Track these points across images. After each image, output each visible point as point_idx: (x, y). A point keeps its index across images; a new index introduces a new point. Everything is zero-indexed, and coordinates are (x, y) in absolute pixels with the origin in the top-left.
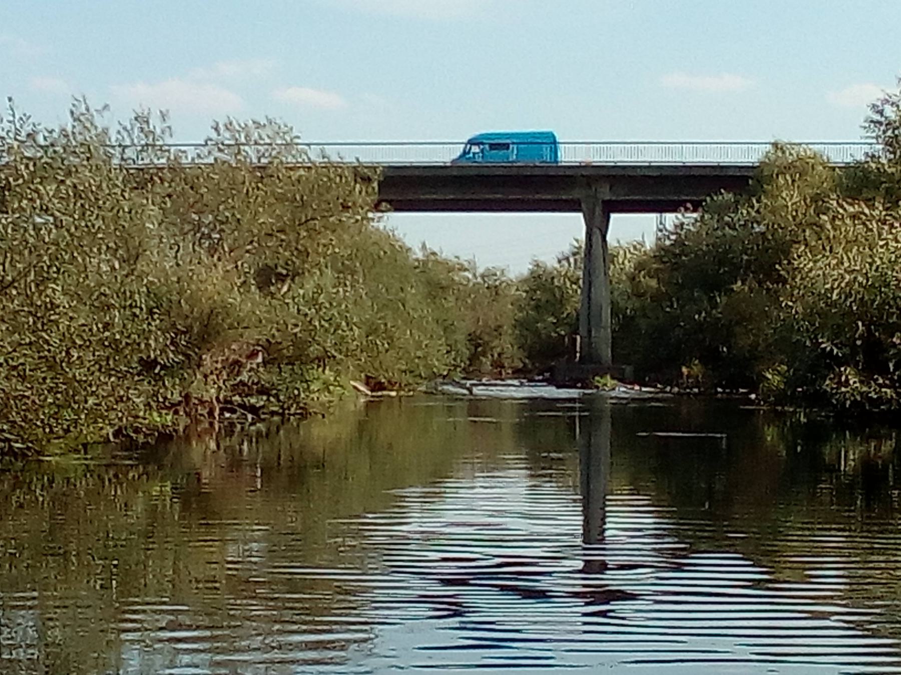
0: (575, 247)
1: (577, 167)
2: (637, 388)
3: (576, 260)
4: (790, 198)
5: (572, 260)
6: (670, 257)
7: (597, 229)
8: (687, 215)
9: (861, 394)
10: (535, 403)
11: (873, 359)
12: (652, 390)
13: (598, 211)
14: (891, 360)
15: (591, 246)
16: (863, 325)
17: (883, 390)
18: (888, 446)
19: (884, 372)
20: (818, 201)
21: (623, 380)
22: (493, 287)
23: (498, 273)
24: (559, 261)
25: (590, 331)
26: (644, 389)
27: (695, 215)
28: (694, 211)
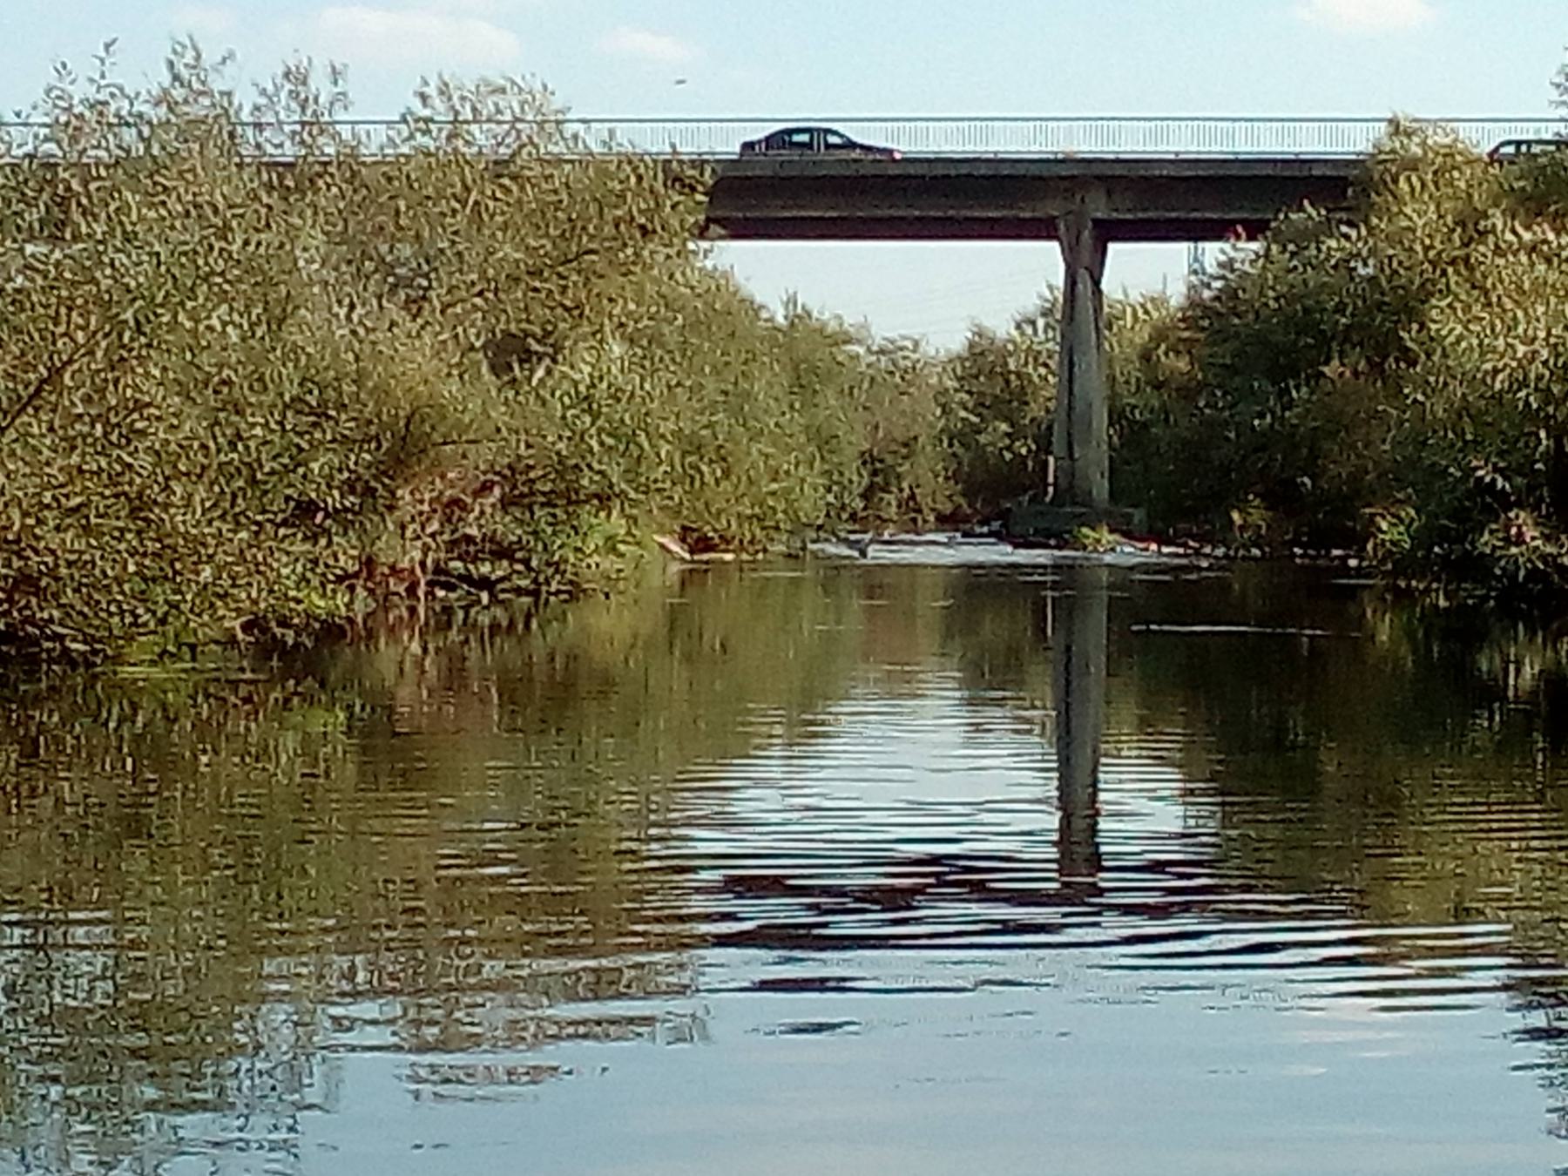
0: (1047, 301)
2: (1154, 547)
4: (1419, 216)
6: (1212, 317)
7: (1084, 270)
12: (1181, 551)
20: (1471, 225)
22: (898, 370)
26: (1165, 550)
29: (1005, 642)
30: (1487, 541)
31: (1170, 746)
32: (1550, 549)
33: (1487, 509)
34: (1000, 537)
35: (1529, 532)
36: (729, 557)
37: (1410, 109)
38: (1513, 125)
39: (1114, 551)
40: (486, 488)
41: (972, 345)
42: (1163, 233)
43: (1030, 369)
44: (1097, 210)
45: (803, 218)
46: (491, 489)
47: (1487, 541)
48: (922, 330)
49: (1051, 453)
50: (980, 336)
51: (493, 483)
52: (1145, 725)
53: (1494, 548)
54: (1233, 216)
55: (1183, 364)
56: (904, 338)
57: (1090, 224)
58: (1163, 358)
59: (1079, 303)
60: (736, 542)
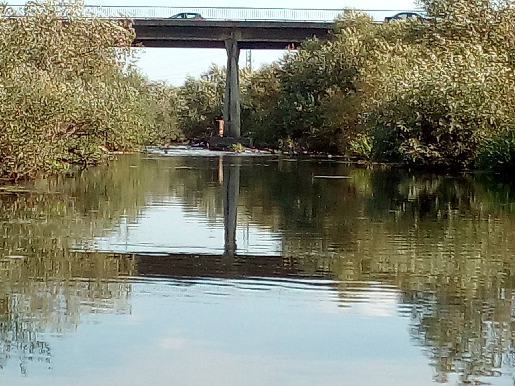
0: (212, 69)
1: (244, 22)
2: (257, 151)
3: (212, 77)
4: (353, 40)
5: (209, 77)
6: (284, 74)
7: (233, 58)
8: (291, 51)
9: (421, 154)
10: (188, 160)
11: (427, 135)
12: (266, 152)
13: (235, 47)
14: (438, 135)
15: (230, 67)
16: (420, 114)
17: (433, 152)
18: (435, 185)
19: (434, 141)
20: (368, 43)
21: (247, 146)
22: (162, 93)
23: (162, 84)
24: (202, 77)
25: (229, 119)
26: (262, 152)
27: (296, 51)
28: (295, 49)
29: (198, 183)
30: (401, 149)
31: (276, 218)
32: (422, 151)
33: (400, 138)
34: (205, 147)
35: (416, 146)
36: (122, 153)
37: (350, 6)
38: (197, 9)
39: (244, 152)
40: (70, 128)
41: (186, 84)
42: (245, 47)
43: (206, 91)
44: (239, 38)
45: (198, 41)
46: (72, 128)
47: (401, 149)
48: (166, 78)
49: (222, 119)
50: (189, 80)
51: (73, 126)
52: (249, 212)
53: (404, 151)
54: (291, 41)
55: (262, 90)
56: (159, 81)
57: (236, 43)
58: (256, 88)
59: (232, 69)
60: (125, 148)
